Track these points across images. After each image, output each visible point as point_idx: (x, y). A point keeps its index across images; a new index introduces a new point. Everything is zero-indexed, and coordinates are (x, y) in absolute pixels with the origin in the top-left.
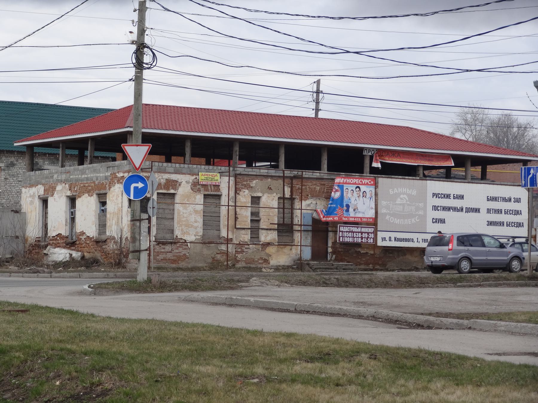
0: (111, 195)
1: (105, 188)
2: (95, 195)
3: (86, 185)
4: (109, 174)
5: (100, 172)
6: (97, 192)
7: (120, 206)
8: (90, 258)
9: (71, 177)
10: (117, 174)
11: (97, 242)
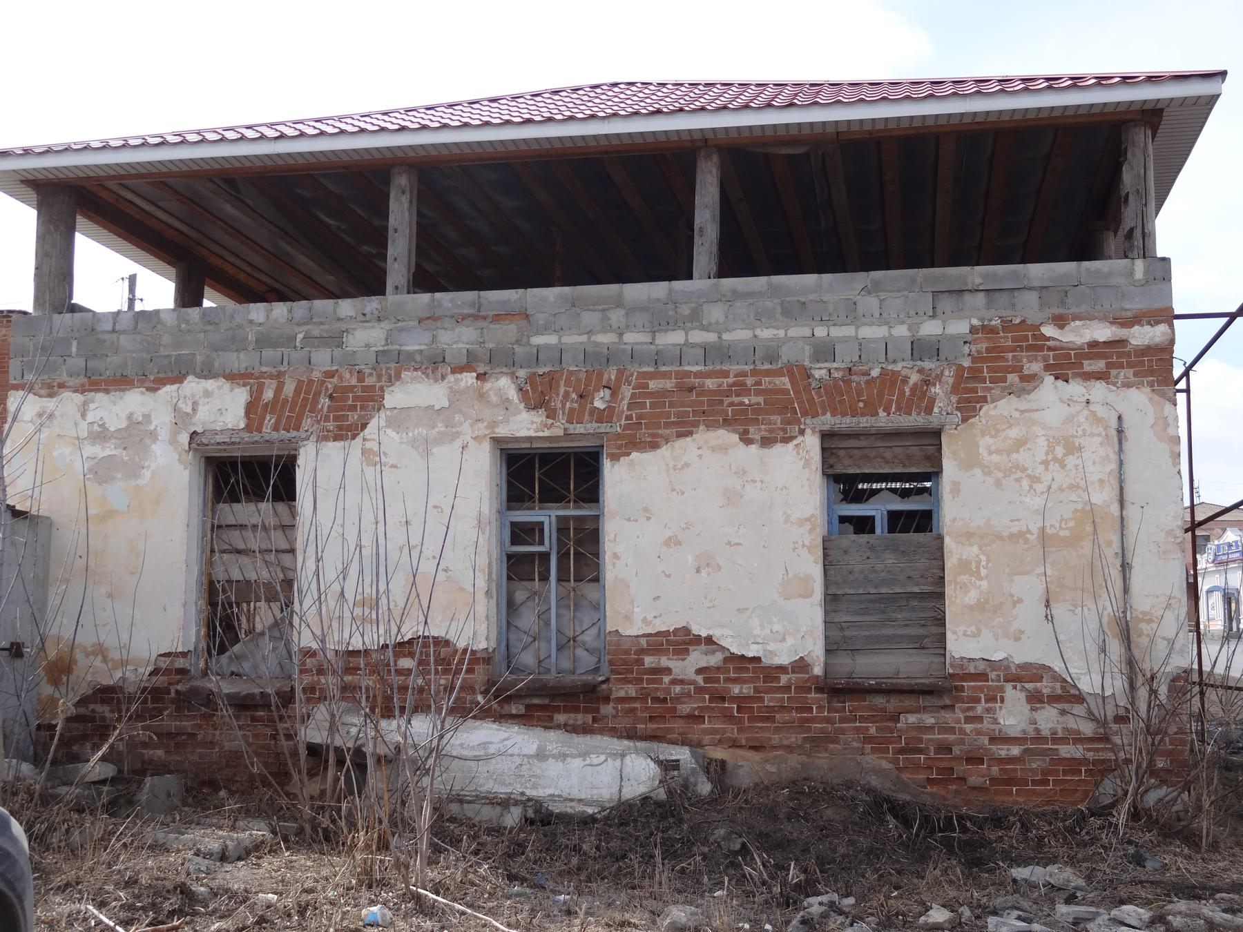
0: (985, 442)
1: (921, 398)
2: (812, 442)
3: (710, 383)
4: (960, 327)
5: (852, 314)
6: (828, 421)
7: (1103, 497)
8: (761, 788)
9: (538, 340)
10: (1048, 330)
11: (838, 690)
